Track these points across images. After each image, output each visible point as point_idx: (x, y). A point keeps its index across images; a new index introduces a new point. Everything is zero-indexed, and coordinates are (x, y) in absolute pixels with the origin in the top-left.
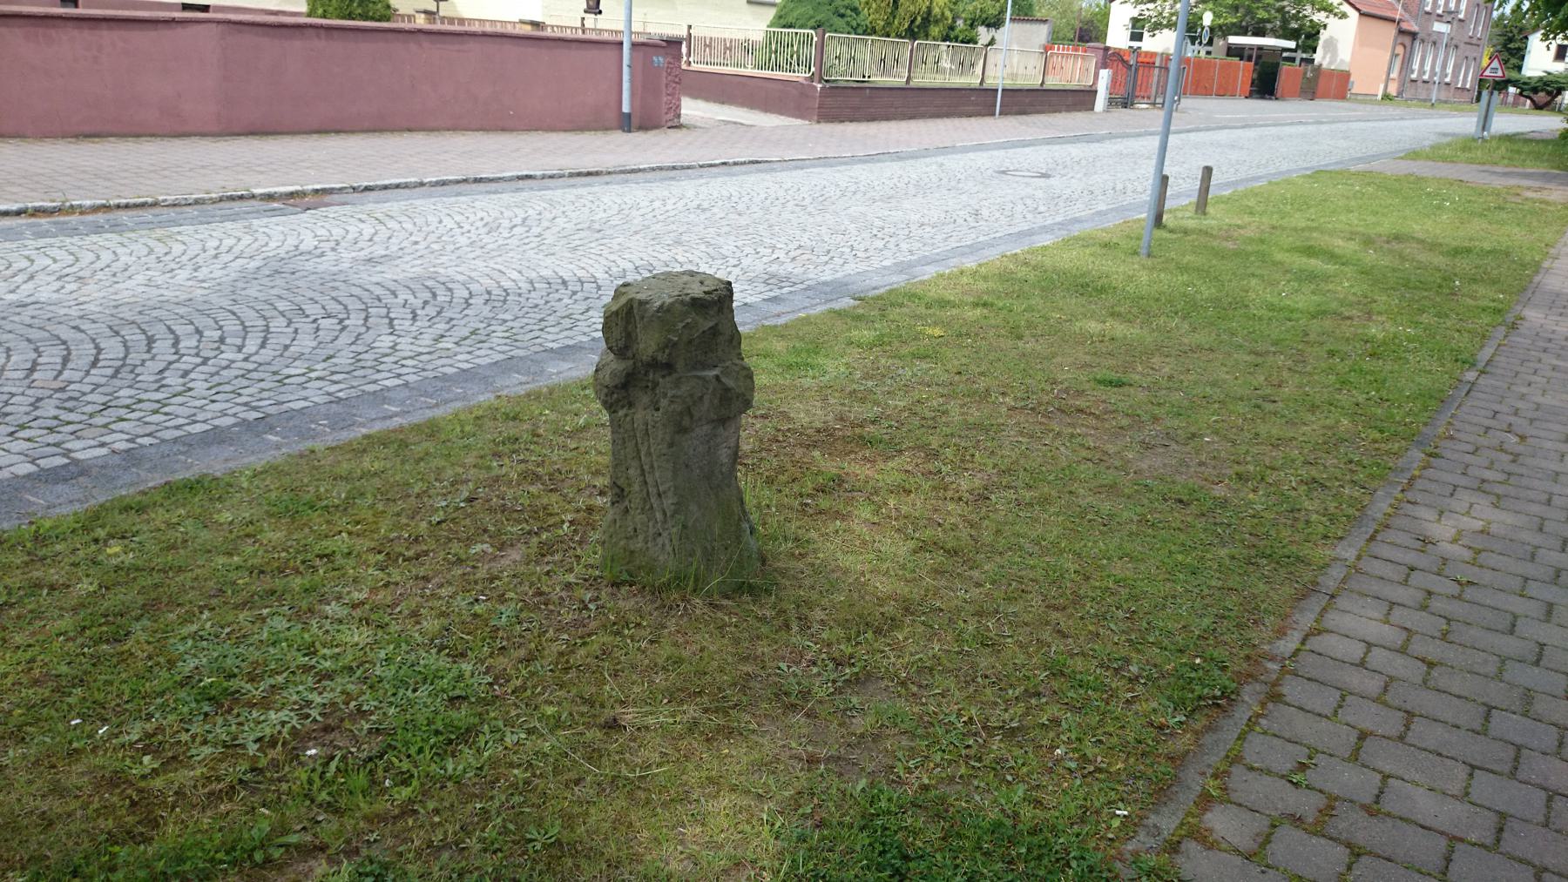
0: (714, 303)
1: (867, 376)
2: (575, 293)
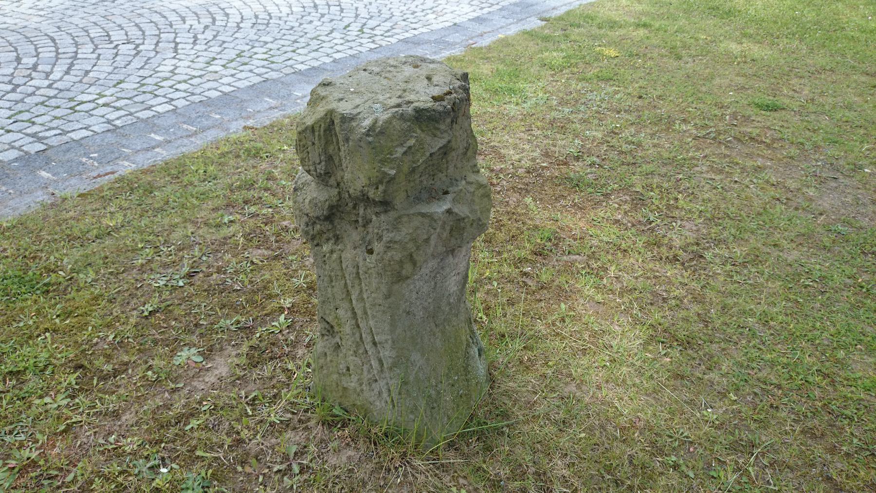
0: (446, 113)
1: (562, 102)
2: (323, 15)
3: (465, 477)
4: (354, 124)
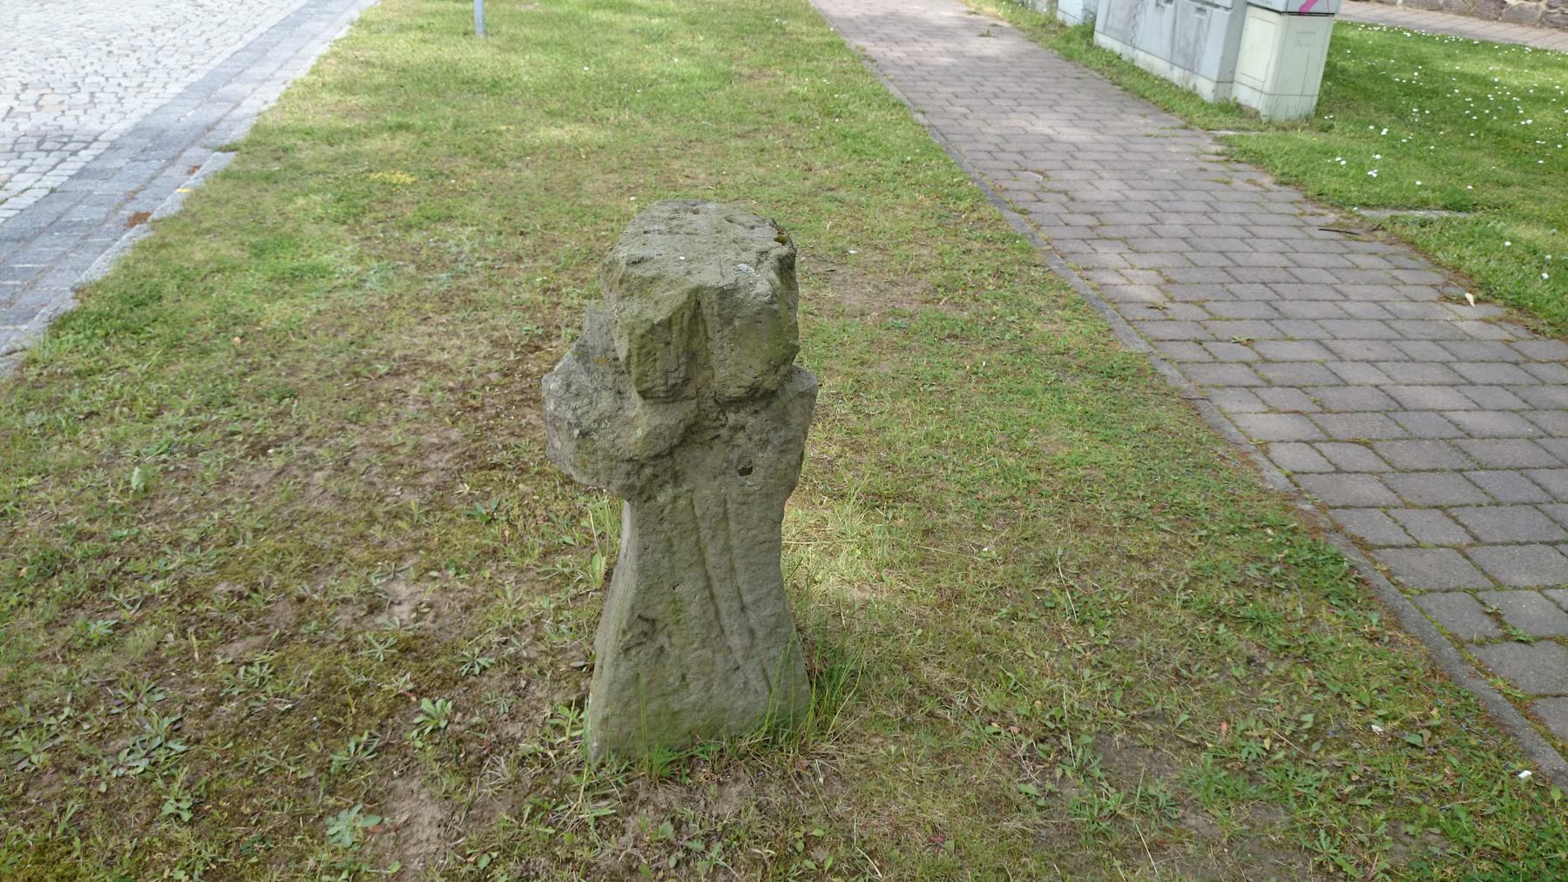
3: (876, 735)
4: (740, 296)
